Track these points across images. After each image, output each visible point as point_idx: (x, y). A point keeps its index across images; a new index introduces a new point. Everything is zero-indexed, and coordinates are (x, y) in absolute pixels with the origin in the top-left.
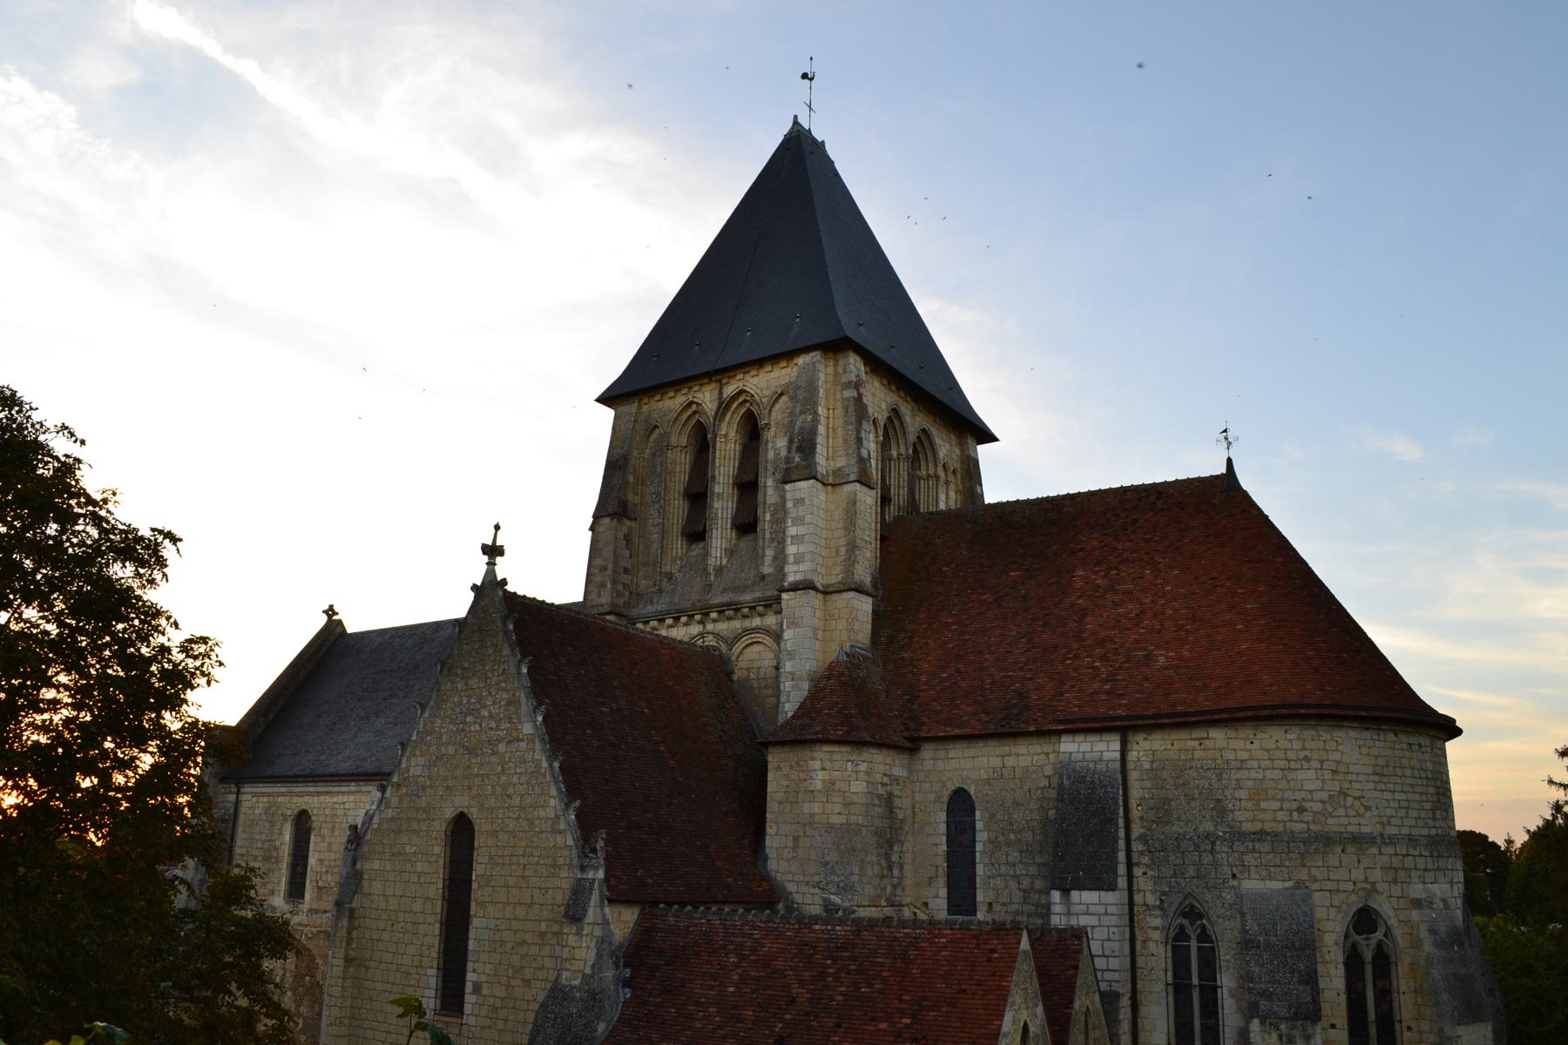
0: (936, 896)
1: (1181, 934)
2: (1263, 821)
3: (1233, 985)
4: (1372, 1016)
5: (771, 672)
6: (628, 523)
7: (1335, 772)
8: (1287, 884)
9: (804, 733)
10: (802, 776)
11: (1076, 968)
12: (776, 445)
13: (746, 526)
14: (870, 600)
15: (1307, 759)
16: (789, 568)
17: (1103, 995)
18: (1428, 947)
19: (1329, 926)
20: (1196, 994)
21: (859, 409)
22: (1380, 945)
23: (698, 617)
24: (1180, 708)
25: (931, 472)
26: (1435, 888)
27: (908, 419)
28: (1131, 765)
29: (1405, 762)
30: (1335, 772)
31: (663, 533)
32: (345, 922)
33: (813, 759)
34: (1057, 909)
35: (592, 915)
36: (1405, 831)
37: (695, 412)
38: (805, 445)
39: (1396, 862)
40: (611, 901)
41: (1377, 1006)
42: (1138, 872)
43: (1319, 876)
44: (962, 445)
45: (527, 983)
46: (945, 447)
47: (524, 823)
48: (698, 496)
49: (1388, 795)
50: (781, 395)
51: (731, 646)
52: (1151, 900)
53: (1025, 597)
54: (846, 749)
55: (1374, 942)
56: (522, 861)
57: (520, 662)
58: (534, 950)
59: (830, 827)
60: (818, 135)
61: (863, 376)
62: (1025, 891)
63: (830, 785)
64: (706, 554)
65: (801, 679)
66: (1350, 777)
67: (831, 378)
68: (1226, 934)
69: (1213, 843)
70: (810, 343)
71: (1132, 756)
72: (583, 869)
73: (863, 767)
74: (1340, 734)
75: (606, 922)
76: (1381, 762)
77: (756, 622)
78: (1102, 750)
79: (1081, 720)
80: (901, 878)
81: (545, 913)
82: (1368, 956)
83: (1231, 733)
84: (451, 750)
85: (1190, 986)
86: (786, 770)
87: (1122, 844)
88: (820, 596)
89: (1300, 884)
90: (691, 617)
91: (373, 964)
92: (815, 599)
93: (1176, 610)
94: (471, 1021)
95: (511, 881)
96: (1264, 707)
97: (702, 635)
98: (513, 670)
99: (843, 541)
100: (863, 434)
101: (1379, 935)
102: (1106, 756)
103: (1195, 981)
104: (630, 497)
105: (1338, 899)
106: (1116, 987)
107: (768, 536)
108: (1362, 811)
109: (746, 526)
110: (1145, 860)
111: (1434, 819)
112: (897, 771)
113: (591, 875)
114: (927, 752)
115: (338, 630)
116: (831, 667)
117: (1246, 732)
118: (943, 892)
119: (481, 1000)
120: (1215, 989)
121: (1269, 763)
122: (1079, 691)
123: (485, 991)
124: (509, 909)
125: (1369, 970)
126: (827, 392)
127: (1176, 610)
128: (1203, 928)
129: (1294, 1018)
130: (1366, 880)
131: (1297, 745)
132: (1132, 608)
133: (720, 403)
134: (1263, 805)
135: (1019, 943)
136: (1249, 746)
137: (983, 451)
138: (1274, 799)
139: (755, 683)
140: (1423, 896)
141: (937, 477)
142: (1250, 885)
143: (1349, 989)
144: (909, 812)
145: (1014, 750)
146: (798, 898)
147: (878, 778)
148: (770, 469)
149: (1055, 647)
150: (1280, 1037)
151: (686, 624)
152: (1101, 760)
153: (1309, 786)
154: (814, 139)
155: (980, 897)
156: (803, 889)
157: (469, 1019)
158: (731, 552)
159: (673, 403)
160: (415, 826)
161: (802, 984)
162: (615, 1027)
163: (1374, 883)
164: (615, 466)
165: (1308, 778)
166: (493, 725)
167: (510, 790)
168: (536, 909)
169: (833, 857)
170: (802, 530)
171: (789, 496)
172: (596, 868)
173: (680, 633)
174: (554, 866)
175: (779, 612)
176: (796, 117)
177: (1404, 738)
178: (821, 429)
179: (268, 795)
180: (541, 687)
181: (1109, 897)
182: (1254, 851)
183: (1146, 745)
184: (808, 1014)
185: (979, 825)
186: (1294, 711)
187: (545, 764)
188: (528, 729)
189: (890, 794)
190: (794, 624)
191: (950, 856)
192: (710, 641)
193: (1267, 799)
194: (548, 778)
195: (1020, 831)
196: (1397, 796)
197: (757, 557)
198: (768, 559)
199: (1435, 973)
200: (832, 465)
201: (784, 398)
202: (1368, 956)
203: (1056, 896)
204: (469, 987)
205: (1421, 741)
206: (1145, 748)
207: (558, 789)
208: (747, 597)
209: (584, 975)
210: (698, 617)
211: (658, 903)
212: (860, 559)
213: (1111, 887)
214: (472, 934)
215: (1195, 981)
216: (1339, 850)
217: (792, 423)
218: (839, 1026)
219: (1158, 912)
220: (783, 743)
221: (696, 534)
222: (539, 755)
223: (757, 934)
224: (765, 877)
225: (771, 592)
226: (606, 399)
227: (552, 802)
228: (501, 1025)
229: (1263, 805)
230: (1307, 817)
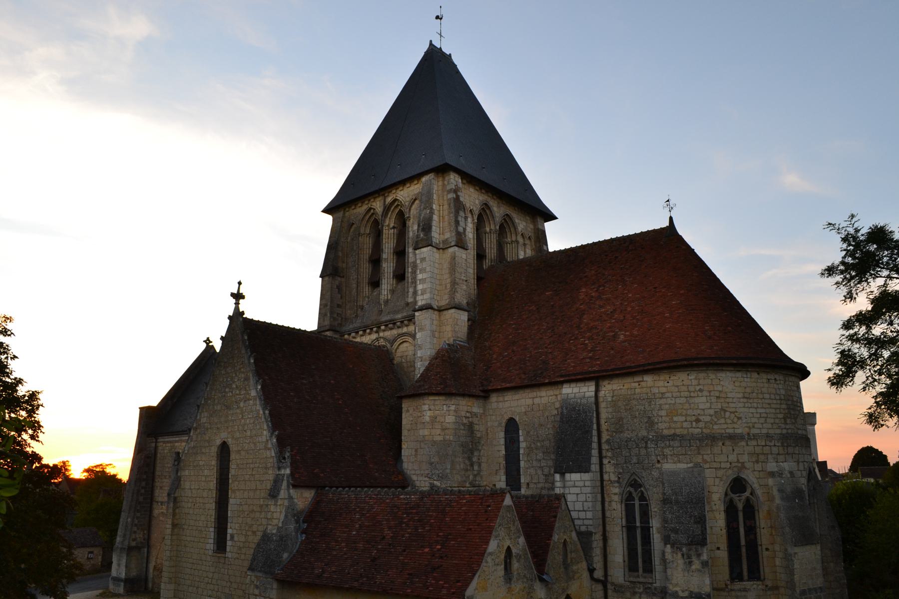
1: (630, 497)
2: (675, 428)
3: (658, 525)
4: (743, 542)
6: (339, 279)
8: (689, 465)
11: (555, 517)
12: (413, 228)
13: (400, 276)
14: (466, 314)
15: (701, 390)
16: (419, 298)
17: (579, 534)
18: (778, 501)
19: (715, 489)
20: (639, 531)
21: (458, 206)
22: (748, 500)
23: (375, 329)
25: (514, 239)
26: (786, 466)
27: (495, 209)
28: (601, 400)
31: (358, 283)
32: (171, 505)
33: (424, 404)
34: (558, 484)
35: (283, 494)
36: (764, 431)
37: (373, 214)
38: (426, 227)
39: (758, 450)
40: (295, 486)
42: (605, 461)
44: (534, 222)
45: (254, 533)
46: (522, 224)
47: (252, 445)
48: (376, 261)
49: (752, 410)
50: (415, 200)
51: (392, 343)
52: (613, 478)
53: (552, 306)
56: (252, 466)
58: (258, 515)
59: (434, 443)
60: (447, 51)
61: (460, 185)
62: (546, 475)
63: (434, 419)
65: (425, 360)
66: (728, 400)
67: (440, 188)
68: (654, 497)
69: (646, 443)
70: (426, 169)
71: (601, 394)
72: (279, 469)
73: (453, 408)
74: (722, 375)
75: (290, 498)
76: (748, 390)
77: (405, 330)
78: (584, 391)
80: (479, 471)
81: (262, 494)
82: (740, 506)
83: (656, 377)
84: (219, 407)
85: (635, 527)
86: (411, 412)
87: (595, 445)
90: (372, 329)
91: (186, 527)
96: (674, 361)
97: (377, 339)
98: (246, 361)
99: (449, 280)
100: (460, 219)
101: (747, 494)
102: (587, 394)
103: (638, 524)
104: (340, 264)
105: (720, 473)
106: (591, 529)
108: (736, 420)
109: (400, 276)
110: (609, 454)
111: (786, 423)
112: (475, 410)
113: (282, 472)
114: (494, 398)
115: (212, 351)
116: (438, 353)
117: (664, 376)
118: (504, 478)
120: (648, 529)
123: (236, 539)
124: (246, 493)
126: (438, 196)
128: (642, 493)
130: (738, 461)
131: (695, 382)
133: (385, 208)
134: (675, 419)
135: (503, 501)
136: (666, 384)
137: (549, 226)
138: (681, 415)
139: (405, 365)
140: (776, 469)
141: (517, 242)
142: (668, 466)
145: (539, 394)
146: (418, 484)
147: (463, 414)
150: (683, 555)
151: (370, 334)
154: (443, 54)
155: (522, 481)
156: (420, 478)
157: (229, 555)
158: (393, 291)
160: (203, 450)
162: (294, 556)
164: (332, 247)
165: (702, 402)
166: (238, 392)
168: (258, 492)
169: (435, 460)
171: (418, 257)
172: (285, 468)
173: (367, 339)
174: (266, 468)
177: (765, 376)
178: (435, 217)
179: (170, 442)
180: (260, 372)
181: (586, 476)
182: (670, 446)
183: (609, 387)
184: (390, 545)
185: (521, 439)
186: (691, 362)
187: (261, 412)
188: (253, 393)
190: (421, 329)
191: (507, 457)
192: (382, 342)
194: (263, 419)
196: (759, 410)
197: (405, 293)
198: (410, 294)
199: (782, 515)
200: (442, 238)
201: (417, 202)
202: (740, 506)
204: (228, 537)
205: (777, 377)
206: (609, 388)
207: (268, 425)
208: (399, 316)
209: (279, 528)
211: (325, 487)
212: (459, 290)
214: (229, 508)
215: (638, 524)
216: (721, 444)
217: (420, 215)
218: (404, 551)
219: (616, 485)
221: (375, 284)
224: (401, 473)
225: (410, 313)
227: (265, 433)
228: (243, 557)
229: (675, 419)
230: (701, 425)
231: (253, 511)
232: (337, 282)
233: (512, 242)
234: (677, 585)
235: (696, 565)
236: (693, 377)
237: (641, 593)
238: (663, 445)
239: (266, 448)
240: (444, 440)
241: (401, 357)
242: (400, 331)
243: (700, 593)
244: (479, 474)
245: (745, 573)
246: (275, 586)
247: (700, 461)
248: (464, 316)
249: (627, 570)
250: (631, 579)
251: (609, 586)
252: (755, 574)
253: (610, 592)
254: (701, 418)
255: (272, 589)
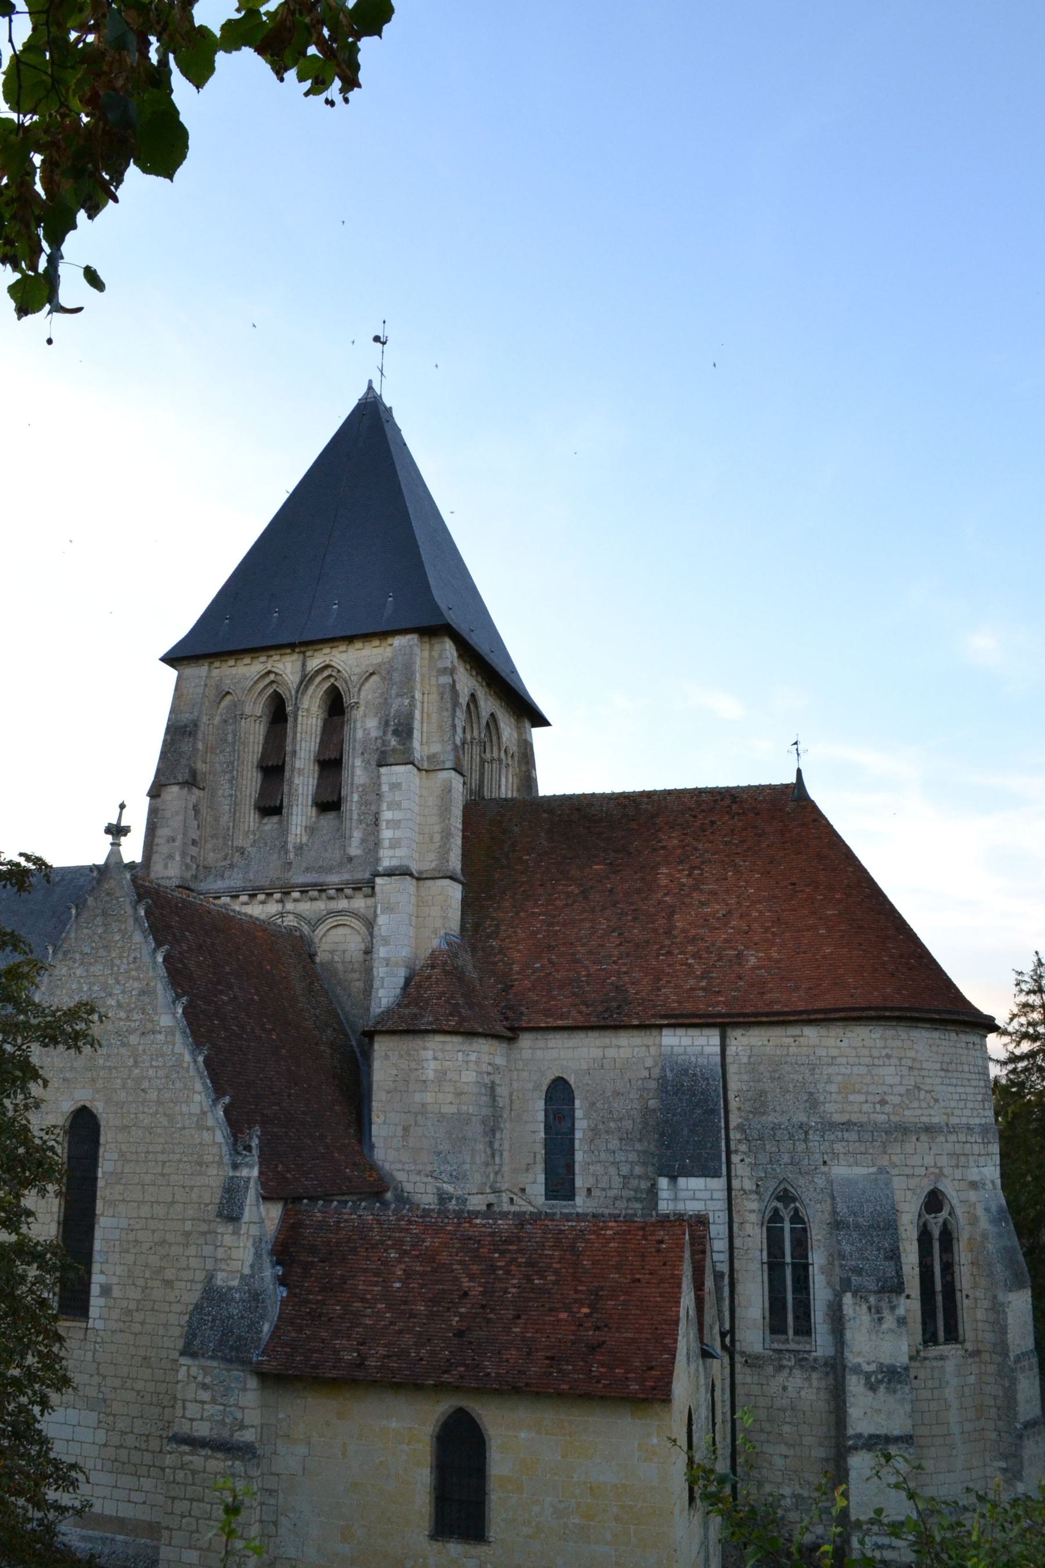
0: (534, 1182)
1: (776, 1216)
4: (938, 1287)
5: (358, 956)
7: (911, 1068)
9: (410, 1021)
10: (413, 1065)
12: (364, 725)
13: (329, 803)
15: (888, 1057)
20: (789, 1271)
22: (945, 1223)
23: (277, 896)
24: (777, 1007)
25: (495, 755)
26: (985, 1170)
29: (964, 1059)
30: (911, 1068)
33: (425, 1049)
34: (664, 1194)
36: (964, 1120)
37: (273, 682)
40: (264, 1198)
41: (943, 1277)
42: (735, 1159)
43: (898, 1163)
44: (520, 729)
45: (168, 1283)
48: (273, 770)
49: (951, 1089)
50: (372, 674)
51: (314, 927)
52: (749, 1185)
53: (611, 891)
54: (457, 1039)
55: (941, 1220)
56: (160, 1157)
57: (155, 951)
59: (442, 1117)
60: (388, 401)
62: (624, 1177)
63: (442, 1076)
64: (284, 831)
65: (397, 964)
66: (923, 1073)
69: (806, 1133)
71: (731, 1050)
72: (235, 1166)
73: (473, 1057)
76: (947, 1059)
78: (699, 1045)
79: (682, 1016)
81: (190, 1213)
82: (936, 1233)
83: (823, 1031)
88: (414, 882)
89: (882, 1170)
92: (409, 883)
93: (760, 912)
94: (99, 1325)
95: (148, 1179)
97: (282, 915)
98: (147, 959)
99: (437, 828)
101: (944, 1214)
102: (708, 1050)
103: (788, 1259)
105: (913, 1183)
107: (355, 817)
108: (932, 1103)
109: (329, 803)
110: (743, 1148)
112: (500, 1061)
113: (245, 1172)
114: (526, 1041)
118: (541, 1178)
119: (111, 1303)
120: (806, 1267)
121: (857, 1060)
122: (676, 987)
123: (116, 1292)
125: (936, 1246)
126: (423, 675)
127: (760, 912)
128: (796, 1210)
129: (882, 1291)
130: (935, 1166)
131: (880, 1043)
132: (718, 908)
134: (851, 1098)
136: (839, 1044)
137: (537, 734)
138: (859, 1092)
139: (340, 967)
141: (500, 760)
142: (840, 1171)
143: (921, 1264)
144: (507, 1100)
145: (615, 1041)
146: (408, 1187)
148: (359, 748)
149: (647, 942)
150: (870, 1308)
151: (263, 903)
152: (702, 1054)
153: (889, 1080)
155: (579, 1182)
158: (311, 830)
159: (249, 670)
161: (472, 1277)
163: (941, 1168)
164: (179, 733)
166: (122, 1015)
167: (145, 1084)
170: (398, 815)
171: (384, 779)
172: (251, 1167)
173: (260, 910)
175: (373, 894)
176: (370, 382)
177: (963, 1037)
178: (417, 714)
182: (842, 1140)
183: (744, 1040)
184: (483, 1307)
185: (578, 1114)
186: (882, 1013)
187: (187, 1058)
188: (166, 1020)
189: (493, 1082)
190: (389, 909)
191: (548, 1144)
192: (290, 921)
193: (854, 1092)
195: (620, 1120)
197: (342, 837)
200: (427, 751)
201: (374, 678)
202: (936, 1233)
203: (663, 1182)
204: (95, 1290)
206: (744, 1043)
207: (204, 1084)
208: (334, 879)
209: (243, 1277)
210: (277, 896)
211: (300, 1199)
213: (717, 1175)
214: (98, 1234)
215: (788, 1259)
216: (914, 1138)
218: (518, 1317)
219: (754, 1196)
220: (393, 1032)
221: (271, 807)
222: (181, 1048)
223: (415, 1229)
224: (373, 1167)
226: (171, 659)
227: (197, 1098)
228: (137, 1328)
229: (851, 1098)
230: (888, 1108)
231: (163, 1242)
232: (193, 799)
233: (493, 760)
234: (859, 1353)
235: (890, 1322)
236: (878, 1035)
237: (791, 1368)
238: (832, 1137)
239: (201, 1127)
240: (459, 1113)
241: (332, 952)
242: (333, 905)
243: (894, 1366)
244: (500, 1170)
245: (941, 1334)
246: (253, 1383)
247: (886, 1163)
248: (455, 892)
249: (767, 1332)
250: (776, 1346)
251: (738, 1358)
252: (952, 1335)
253: (738, 1367)
254: (887, 1098)
255: (244, 1389)
